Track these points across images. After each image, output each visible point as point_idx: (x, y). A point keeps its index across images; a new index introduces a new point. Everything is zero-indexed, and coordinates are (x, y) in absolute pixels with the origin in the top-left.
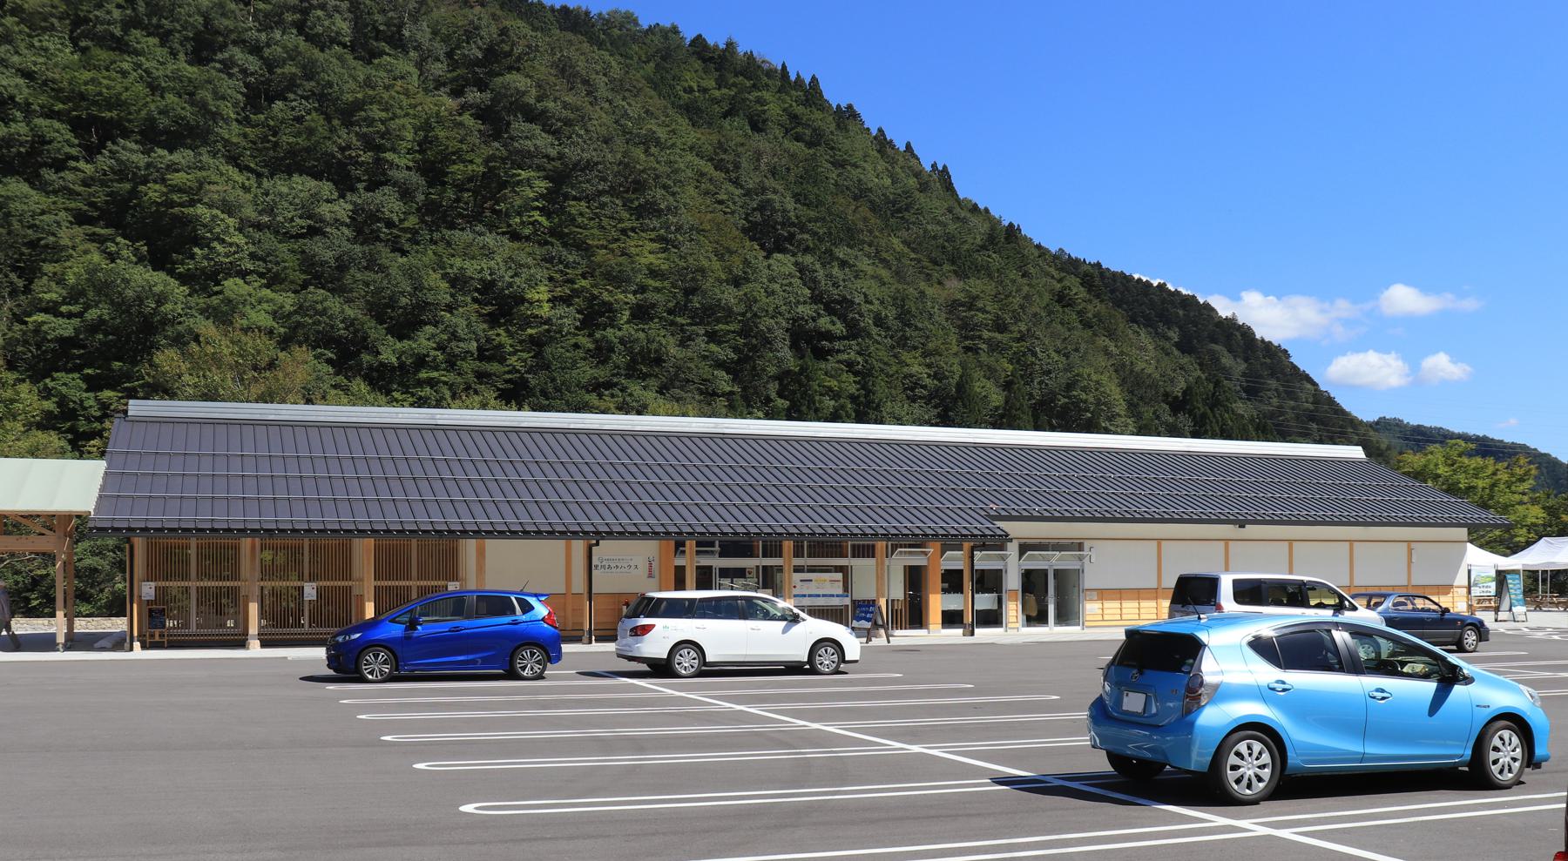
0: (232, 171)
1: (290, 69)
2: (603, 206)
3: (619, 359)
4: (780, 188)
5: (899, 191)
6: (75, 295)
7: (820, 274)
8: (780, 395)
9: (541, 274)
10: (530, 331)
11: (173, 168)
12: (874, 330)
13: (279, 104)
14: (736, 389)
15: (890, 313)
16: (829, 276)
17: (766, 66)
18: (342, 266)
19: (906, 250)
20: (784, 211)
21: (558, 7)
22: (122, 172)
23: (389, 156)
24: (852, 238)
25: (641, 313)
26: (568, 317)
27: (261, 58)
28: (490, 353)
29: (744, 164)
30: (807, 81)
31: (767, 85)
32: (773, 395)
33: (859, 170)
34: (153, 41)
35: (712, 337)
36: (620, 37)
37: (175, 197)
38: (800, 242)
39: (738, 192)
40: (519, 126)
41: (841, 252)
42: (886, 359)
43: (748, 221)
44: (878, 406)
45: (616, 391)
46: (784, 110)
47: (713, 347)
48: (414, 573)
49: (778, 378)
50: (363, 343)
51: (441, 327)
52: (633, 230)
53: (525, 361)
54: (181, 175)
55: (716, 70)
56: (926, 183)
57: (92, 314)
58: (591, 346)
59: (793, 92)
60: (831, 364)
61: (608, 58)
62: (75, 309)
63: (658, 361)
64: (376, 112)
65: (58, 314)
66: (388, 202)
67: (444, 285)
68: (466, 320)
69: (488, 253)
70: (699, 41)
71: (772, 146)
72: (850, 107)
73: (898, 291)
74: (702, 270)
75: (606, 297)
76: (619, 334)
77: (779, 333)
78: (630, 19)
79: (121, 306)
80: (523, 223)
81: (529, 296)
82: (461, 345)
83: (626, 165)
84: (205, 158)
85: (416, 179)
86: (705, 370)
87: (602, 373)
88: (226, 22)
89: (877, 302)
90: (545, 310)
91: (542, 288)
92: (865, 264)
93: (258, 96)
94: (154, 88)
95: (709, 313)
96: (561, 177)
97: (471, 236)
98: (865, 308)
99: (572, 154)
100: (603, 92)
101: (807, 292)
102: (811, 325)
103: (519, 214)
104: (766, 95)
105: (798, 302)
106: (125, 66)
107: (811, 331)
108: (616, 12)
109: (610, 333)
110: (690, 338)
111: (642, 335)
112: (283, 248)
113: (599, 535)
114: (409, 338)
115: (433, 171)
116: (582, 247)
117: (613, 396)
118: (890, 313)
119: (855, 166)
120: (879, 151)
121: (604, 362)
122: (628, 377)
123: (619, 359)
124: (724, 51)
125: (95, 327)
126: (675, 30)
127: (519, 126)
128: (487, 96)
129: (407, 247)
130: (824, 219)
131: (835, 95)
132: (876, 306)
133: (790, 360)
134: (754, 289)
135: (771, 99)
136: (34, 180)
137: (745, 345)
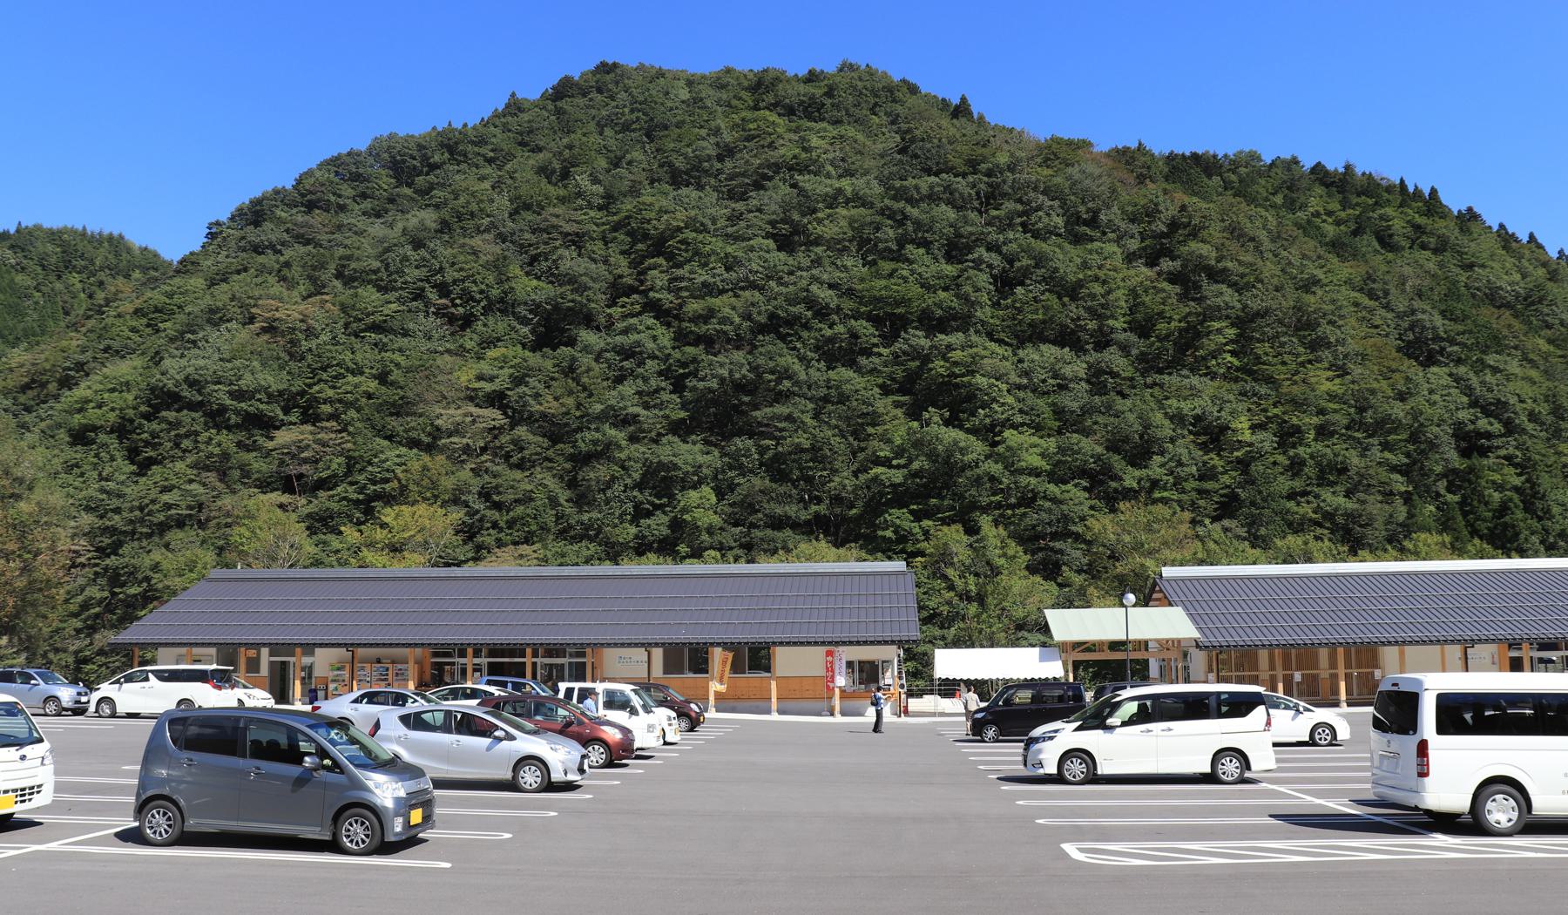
0: (993, 346)
1: (1026, 262)
2: (1282, 345)
3: (1310, 470)
4: (1428, 308)
5: (1531, 286)
6: (899, 453)
7: (1474, 381)
8: (1449, 490)
9: (1242, 407)
10: (1236, 454)
11: (950, 348)
12: (1530, 427)
13: (1019, 290)
14: (1411, 489)
15: (1543, 409)
16: (1483, 383)
17: (1384, 183)
18: (1087, 411)
19: (1552, 348)
20: (1434, 328)
21: (1188, 154)
22: (916, 353)
23: (1111, 322)
24: (1499, 344)
25: (1323, 432)
26: (1266, 440)
27: (1000, 253)
28: (1207, 474)
29: (1393, 291)
30: (1427, 192)
31: (1388, 200)
32: (1443, 492)
33: (1488, 270)
34: (921, 251)
35: (1386, 446)
36: (1248, 175)
37: (956, 371)
38: (1450, 355)
39: (1390, 315)
40: (1209, 288)
41: (1491, 359)
42: (1543, 451)
43: (1403, 341)
44: (1544, 496)
45: (1311, 498)
46: (1408, 222)
47: (1387, 455)
48: (1294, 666)
49: (1444, 475)
50: (1108, 473)
51: (1168, 456)
52: (1310, 362)
53: (1234, 478)
54: (959, 352)
55: (1339, 192)
56: (1555, 270)
57: (916, 465)
58: (1287, 462)
59: (1414, 204)
60: (1491, 460)
61: (1264, 213)
62: (902, 461)
63: (1343, 470)
64: (1098, 289)
65: (890, 467)
66: (1114, 359)
67: (1167, 422)
68: (1185, 448)
69: (1194, 393)
70: (1318, 169)
71: (1415, 266)
72: (1470, 209)
73: (1549, 389)
74: (1373, 392)
75: (1295, 421)
76: (1308, 450)
77: (1445, 438)
78: (1254, 157)
79: (932, 456)
80: (1218, 364)
81: (1233, 426)
82: (1185, 469)
83: (1298, 308)
84: (974, 338)
85: (1133, 338)
86: (1383, 474)
87: (1298, 484)
88: (970, 229)
89: (1529, 401)
90: (1247, 436)
91: (1243, 419)
92: (1514, 366)
93: (1005, 283)
94: (925, 285)
95: (1382, 426)
96: (1245, 322)
97: (1179, 379)
98: (1519, 407)
99: (1255, 305)
100: (1267, 244)
101: (1465, 399)
102: (1471, 427)
103: (1215, 357)
104: (1389, 211)
105: (1457, 409)
106: (905, 273)
107: (1470, 432)
108: (1241, 152)
109: (1301, 450)
110: (1366, 449)
111: (1328, 451)
112: (1041, 403)
113: (1473, 642)
114: (1146, 467)
115: (1142, 328)
116: (1270, 380)
117: (1308, 502)
118: (1543, 409)
119: (1483, 266)
120: (1504, 248)
121: (1295, 475)
122: (1318, 485)
123: (1310, 470)
124: (1345, 174)
125: (915, 474)
126: (1295, 161)
127: (1209, 288)
128: (1178, 263)
129: (1127, 391)
130: (1470, 332)
131: (1454, 202)
132: (1529, 404)
133: (1457, 461)
134: (1418, 401)
135: (1394, 214)
136: (852, 364)
137: (1415, 451)
